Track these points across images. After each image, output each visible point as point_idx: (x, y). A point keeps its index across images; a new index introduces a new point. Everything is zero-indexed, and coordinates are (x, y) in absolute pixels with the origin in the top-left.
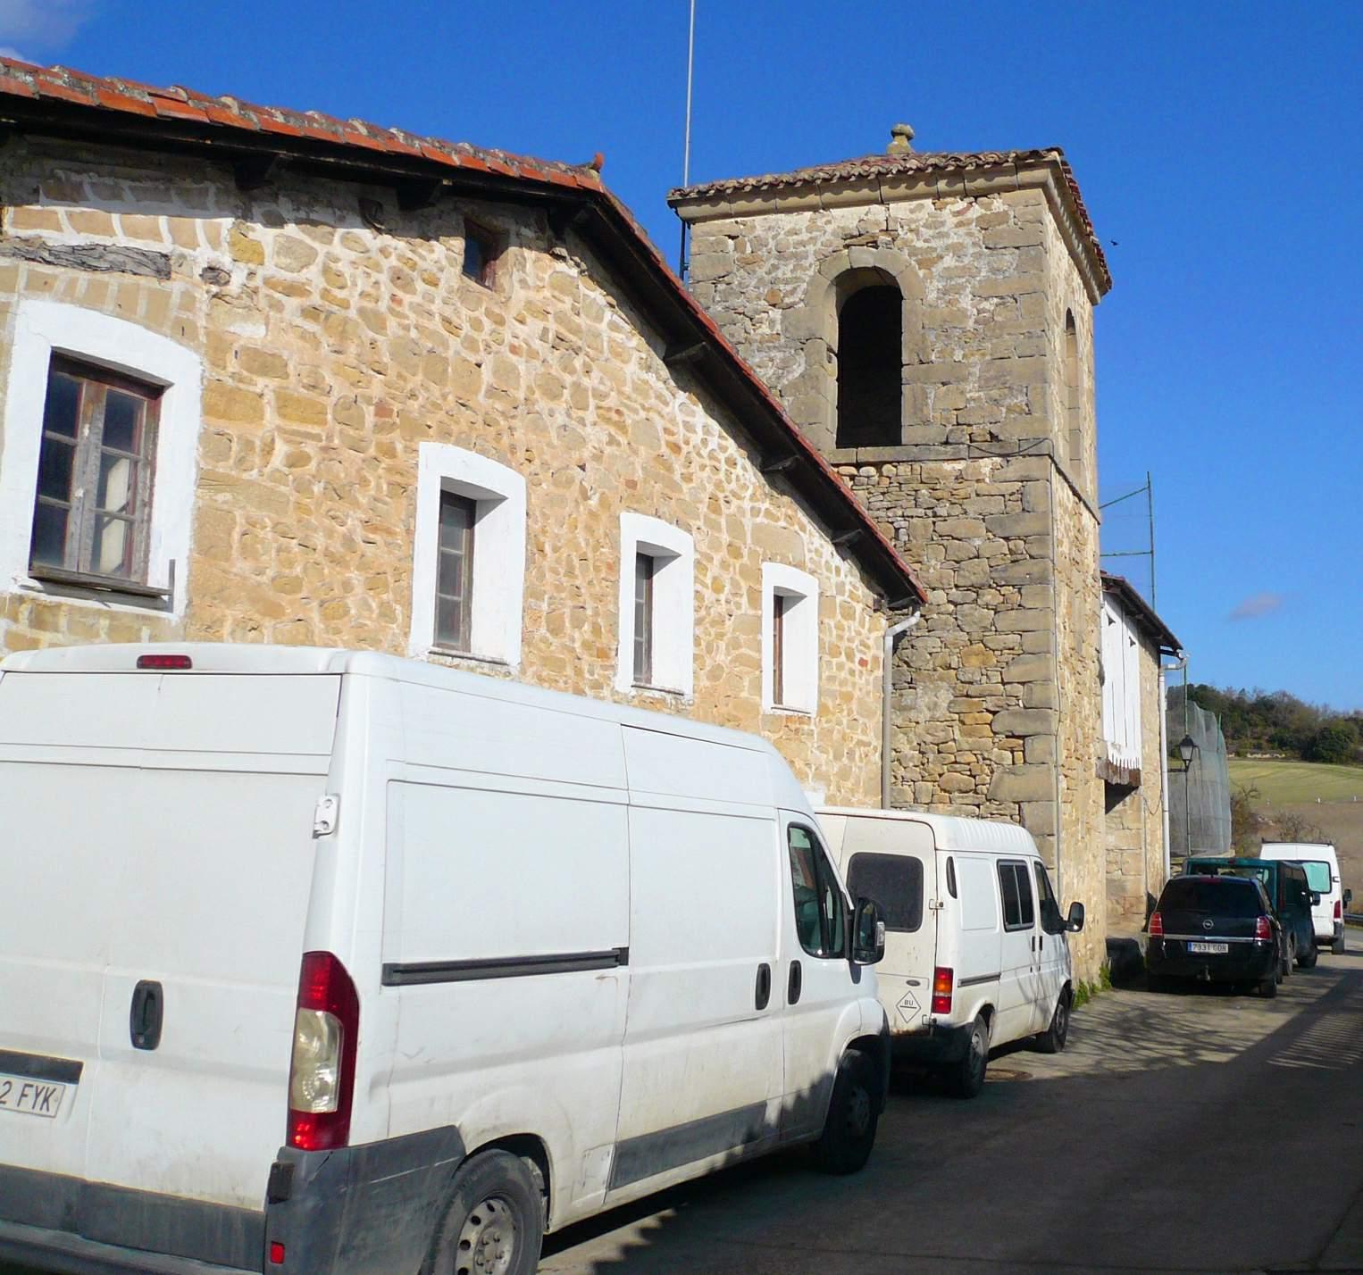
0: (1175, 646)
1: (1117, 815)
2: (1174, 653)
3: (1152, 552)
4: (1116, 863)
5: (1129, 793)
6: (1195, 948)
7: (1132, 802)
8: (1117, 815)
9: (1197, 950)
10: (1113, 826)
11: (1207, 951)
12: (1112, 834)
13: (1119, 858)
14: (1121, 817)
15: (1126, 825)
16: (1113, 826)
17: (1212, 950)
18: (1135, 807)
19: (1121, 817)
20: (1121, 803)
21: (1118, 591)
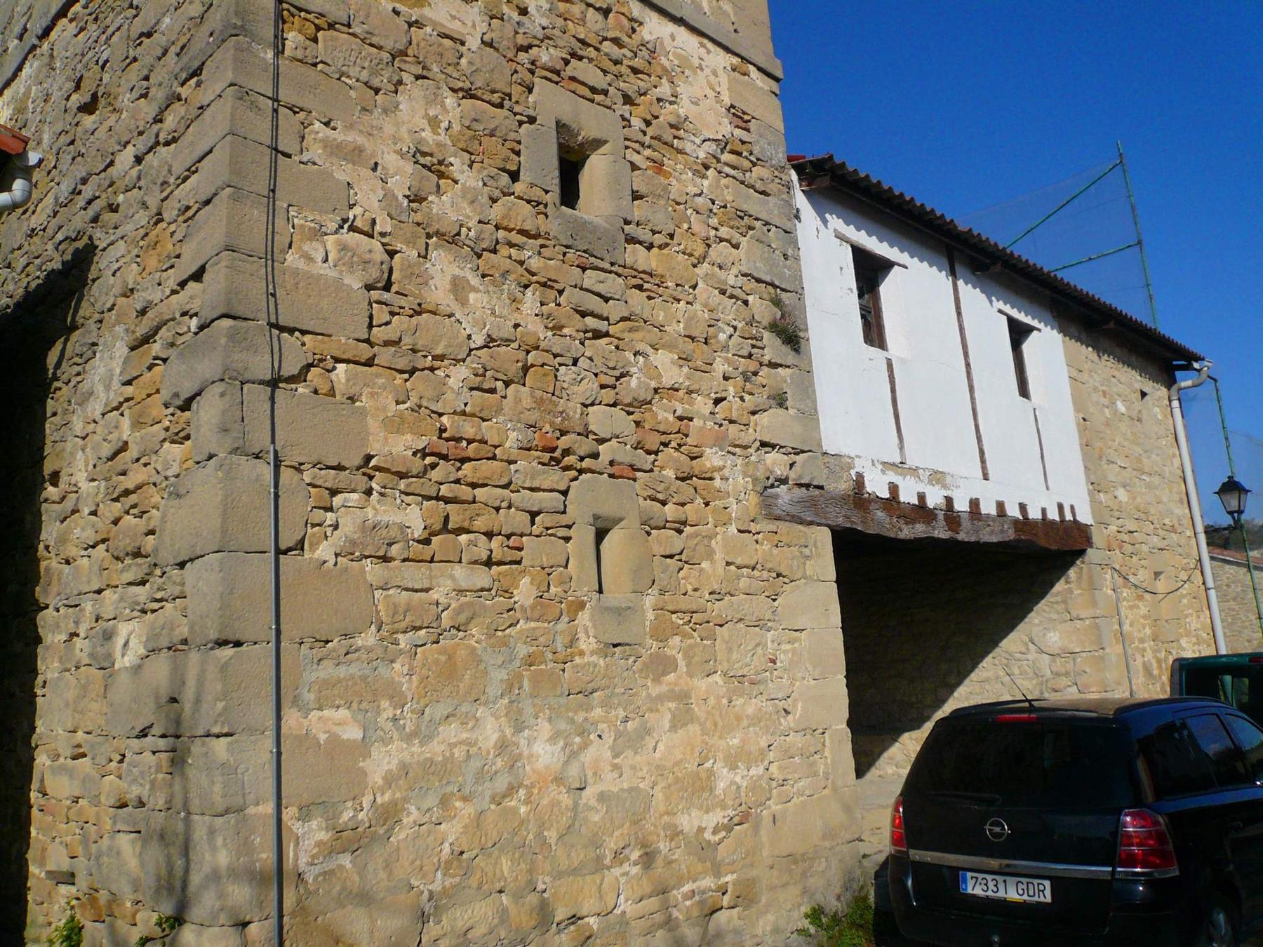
0: (1187, 358)
1: (1059, 599)
2: (1188, 367)
3: (1140, 242)
4: (1067, 674)
5: (1072, 564)
6: (975, 887)
7: (1079, 577)
8: (1059, 599)
9: (978, 891)
10: (1055, 616)
11: (1001, 894)
12: (1054, 629)
13: (1070, 666)
14: (1064, 602)
15: (1074, 614)
16: (1055, 616)
17: (1012, 892)
18: (1085, 584)
19: (1064, 602)
20: (1062, 581)
21: (825, 181)
